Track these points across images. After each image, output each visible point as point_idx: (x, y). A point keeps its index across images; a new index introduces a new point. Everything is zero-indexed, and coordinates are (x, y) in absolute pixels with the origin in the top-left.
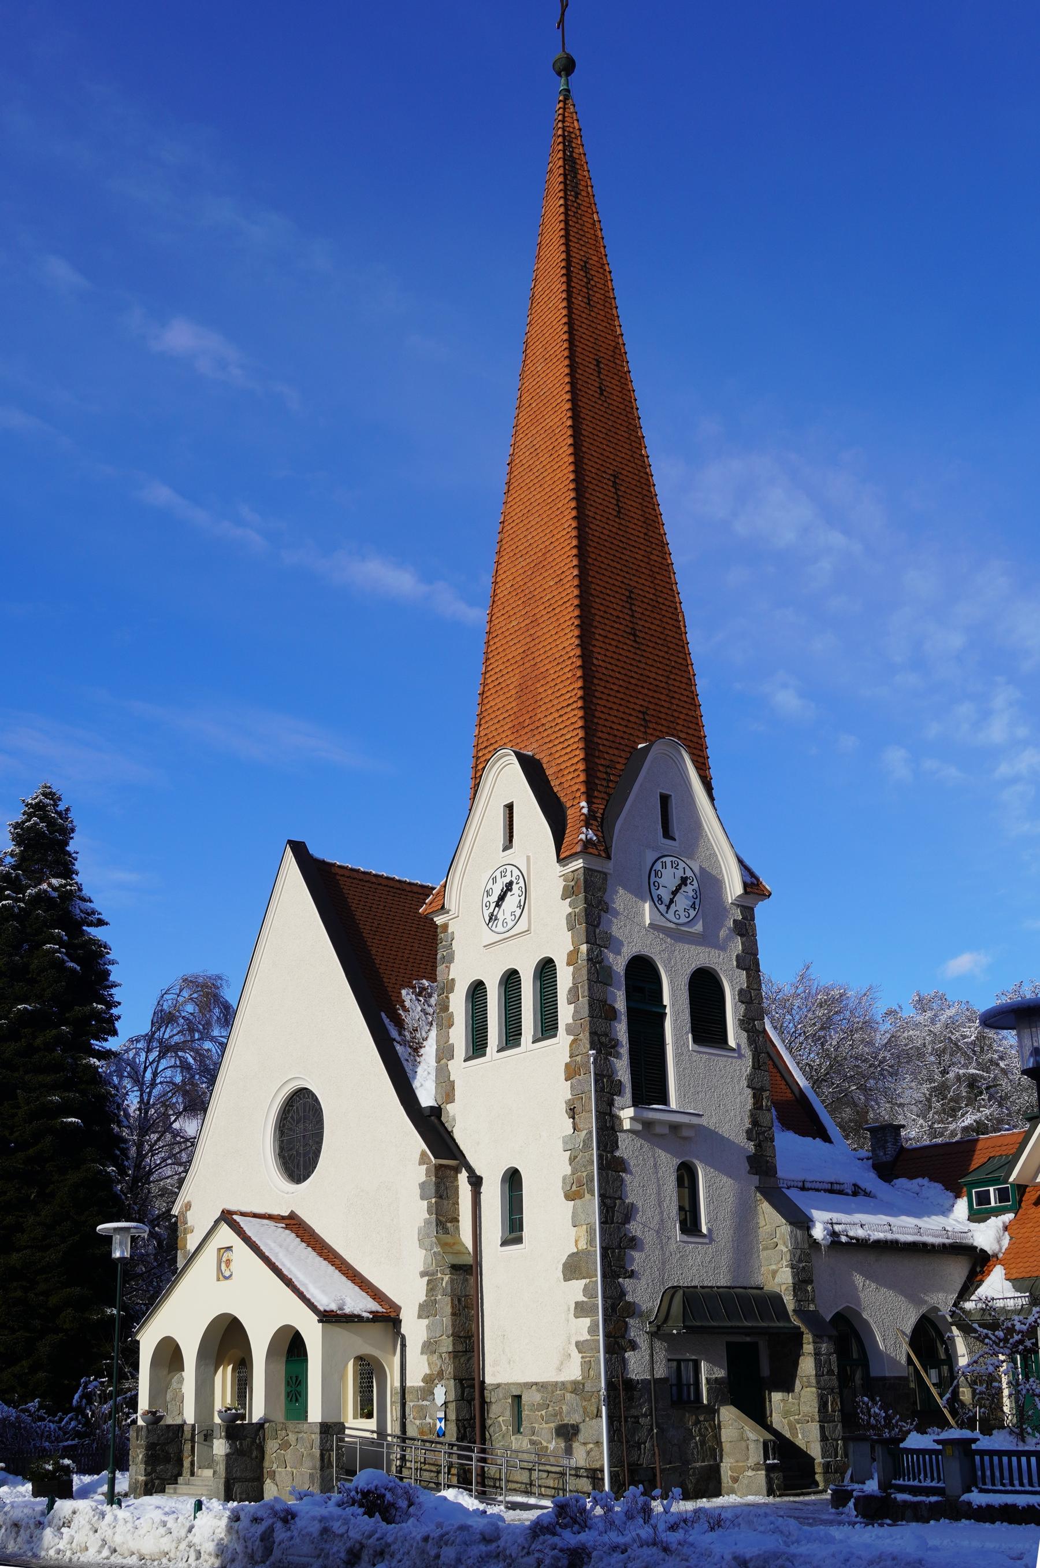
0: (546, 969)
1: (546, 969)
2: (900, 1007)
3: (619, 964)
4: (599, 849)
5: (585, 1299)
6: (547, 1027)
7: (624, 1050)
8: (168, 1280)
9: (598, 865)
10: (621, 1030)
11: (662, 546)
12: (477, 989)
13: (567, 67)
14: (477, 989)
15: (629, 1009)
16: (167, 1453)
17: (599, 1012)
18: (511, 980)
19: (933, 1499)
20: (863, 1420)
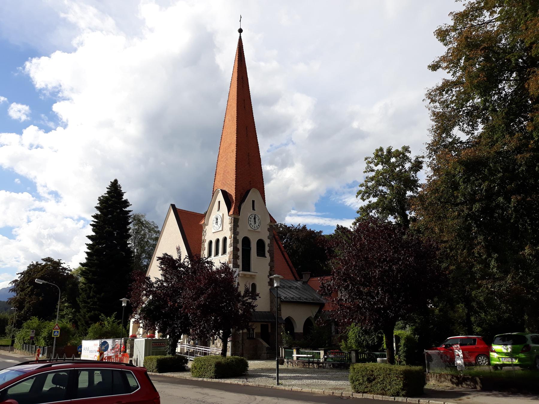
0: (225, 239)
1: (225, 239)
2: (366, 159)
3: (240, 238)
4: (237, 212)
5: (55, 386)
6: (224, 252)
7: (241, 257)
8: (341, 368)
9: (236, 217)
10: (240, 253)
11: (253, 118)
12: (210, 243)
13: (240, 31)
14: (210, 243)
15: (242, 249)
16: (476, 237)
17: (235, 249)
18: (218, 241)
19: (229, 344)
20: (137, 250)
